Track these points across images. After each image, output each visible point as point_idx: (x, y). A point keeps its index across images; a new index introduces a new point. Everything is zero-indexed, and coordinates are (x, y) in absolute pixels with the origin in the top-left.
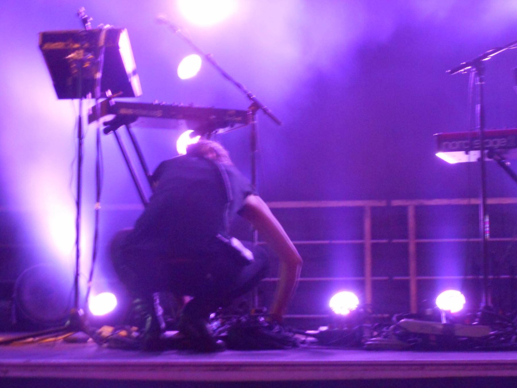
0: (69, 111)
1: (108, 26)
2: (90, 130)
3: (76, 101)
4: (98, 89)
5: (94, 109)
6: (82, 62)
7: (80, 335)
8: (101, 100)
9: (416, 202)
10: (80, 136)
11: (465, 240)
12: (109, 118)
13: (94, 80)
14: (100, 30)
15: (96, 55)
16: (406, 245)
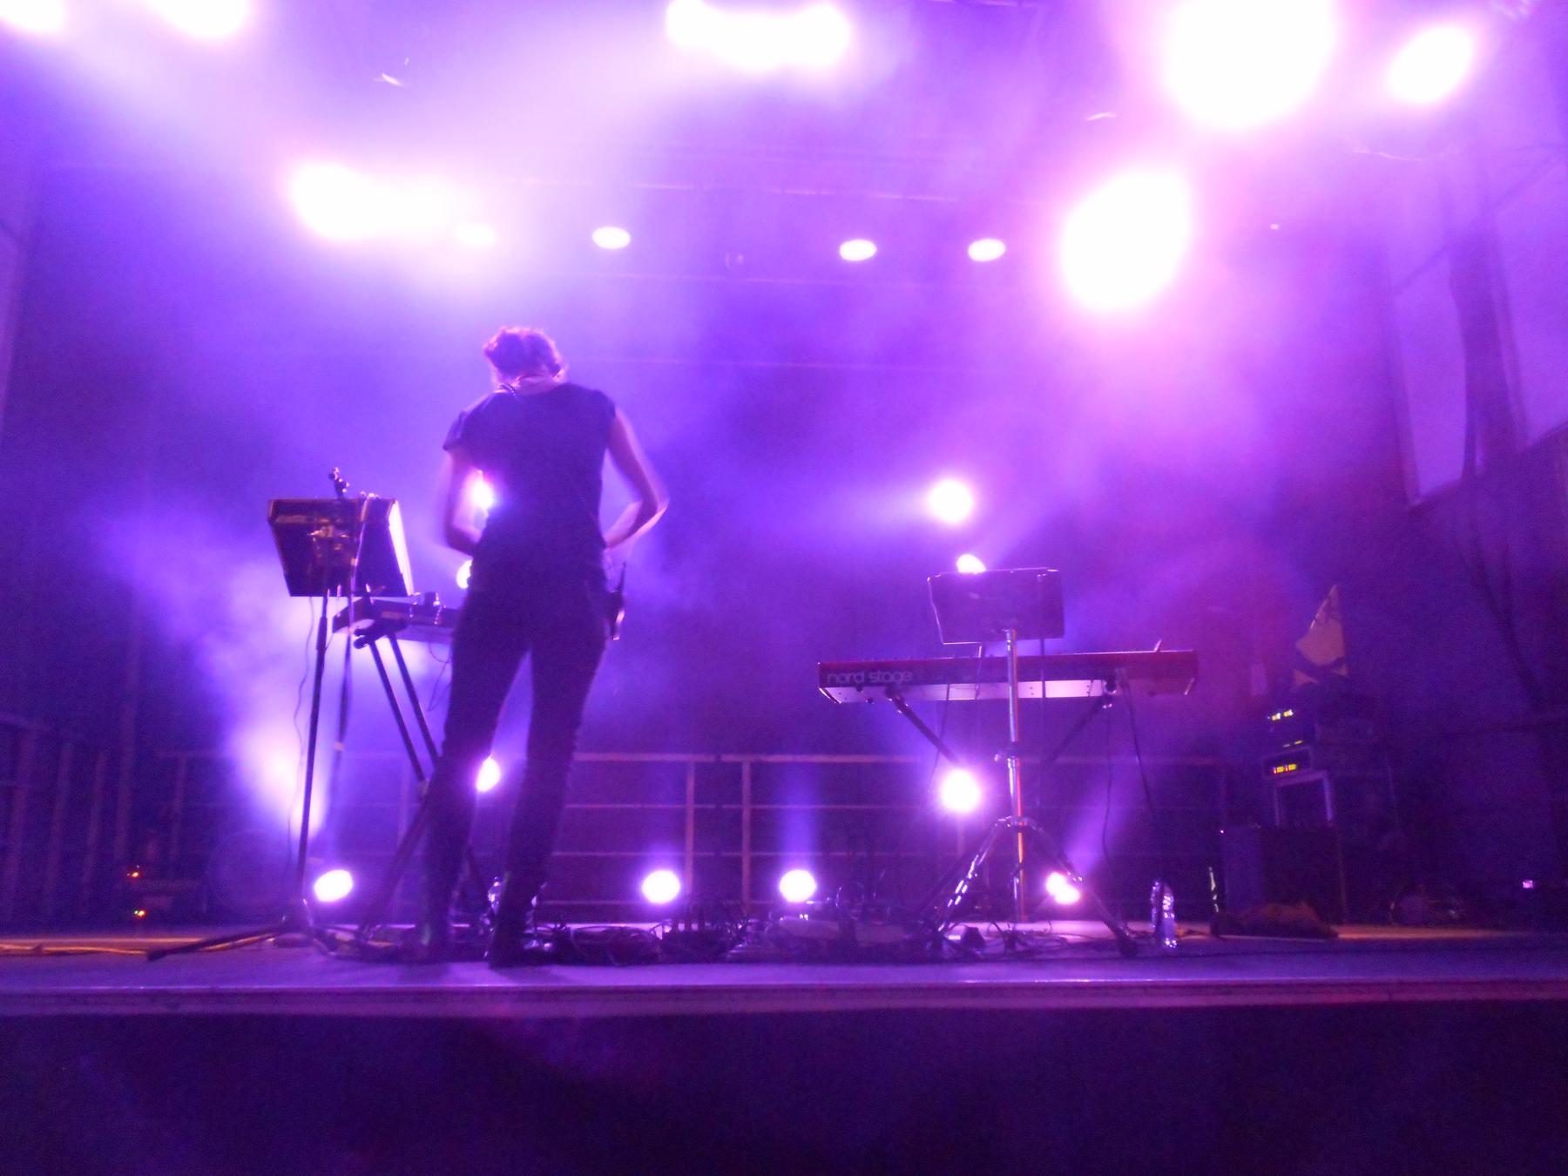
0: (302, 615)
1: (372, 495)
2: (338, 641)
3: (318, 601)
4: (353, 581)
5: (345, 612)
6: (331, 542)
7: (298, 936)
8: (355, 599)
10: (322, 646)
12: (365, 624)
13: (349, 568)
14: (361, 501)
15: (353, 533)
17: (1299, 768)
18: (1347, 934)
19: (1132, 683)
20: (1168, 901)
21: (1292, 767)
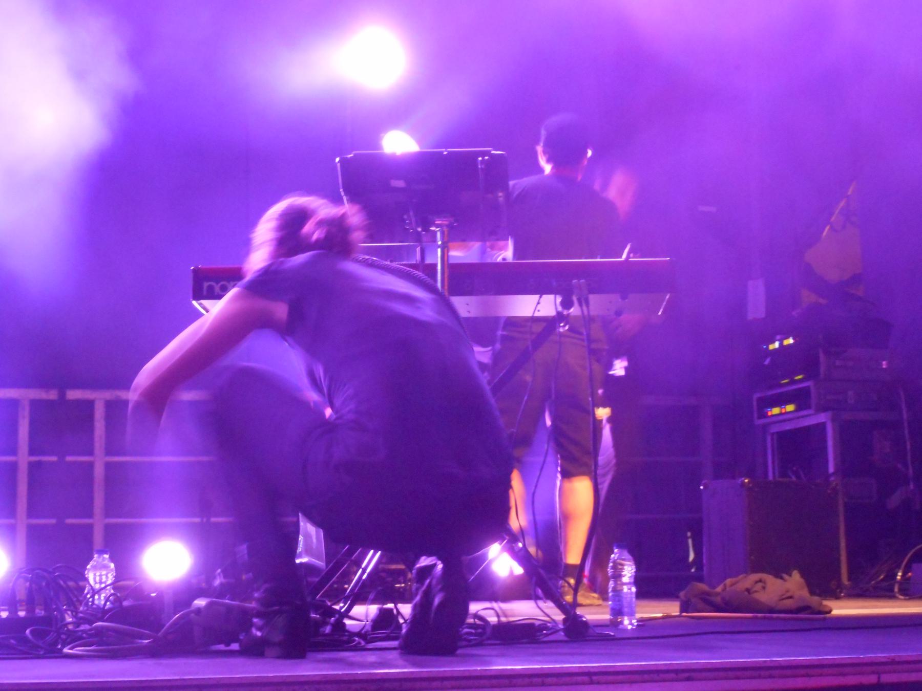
9: (108, 395)
11: (181, 459)
16: (91, 465)
17: (796, 411)
18: (842, 609)
19: (592, 297)
20: (628, 571)
21: (790, 408)
